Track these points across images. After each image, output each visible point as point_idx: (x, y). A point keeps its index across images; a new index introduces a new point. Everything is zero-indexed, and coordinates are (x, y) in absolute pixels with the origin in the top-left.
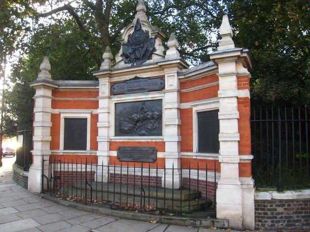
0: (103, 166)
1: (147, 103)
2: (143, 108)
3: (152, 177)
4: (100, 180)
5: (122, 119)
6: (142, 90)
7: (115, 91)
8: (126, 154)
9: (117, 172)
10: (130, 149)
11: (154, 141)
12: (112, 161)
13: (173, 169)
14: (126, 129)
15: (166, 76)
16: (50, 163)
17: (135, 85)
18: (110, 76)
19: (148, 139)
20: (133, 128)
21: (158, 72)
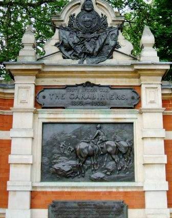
2: (98, 134)
7: (47, 101)
10: (76, 205)
11: (121, 190)
14: (67, 168)
15: (143, 87)
18: (39, 74)
20: (79, 167)
21: (128, 80)
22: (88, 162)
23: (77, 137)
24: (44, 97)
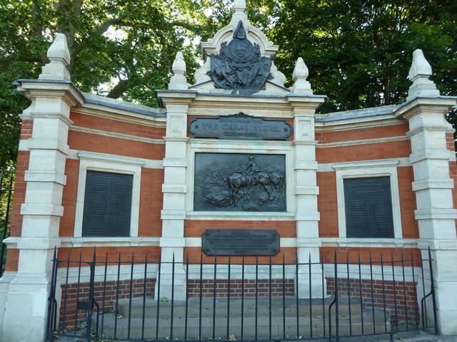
0: (310, 264)
1: (259, 157)
3: (233, 281)
4: (165, 293)
5: (208, 180)
6: (252, 136)
7: (198, 132)
8: (219, 244)
9: (275, 277)
10: (230, 234)
11: (273, 219)
12: (189, 257)
13: (173, 263)
14: (220, 198)
15: (297, 119)
16: (323, 260)
17: (239, 124)
18: (192, 102)
19: (265, 217)
20: (232, 197)
22: (241, 192)
23: (230, 168)
24: (197, 127)
